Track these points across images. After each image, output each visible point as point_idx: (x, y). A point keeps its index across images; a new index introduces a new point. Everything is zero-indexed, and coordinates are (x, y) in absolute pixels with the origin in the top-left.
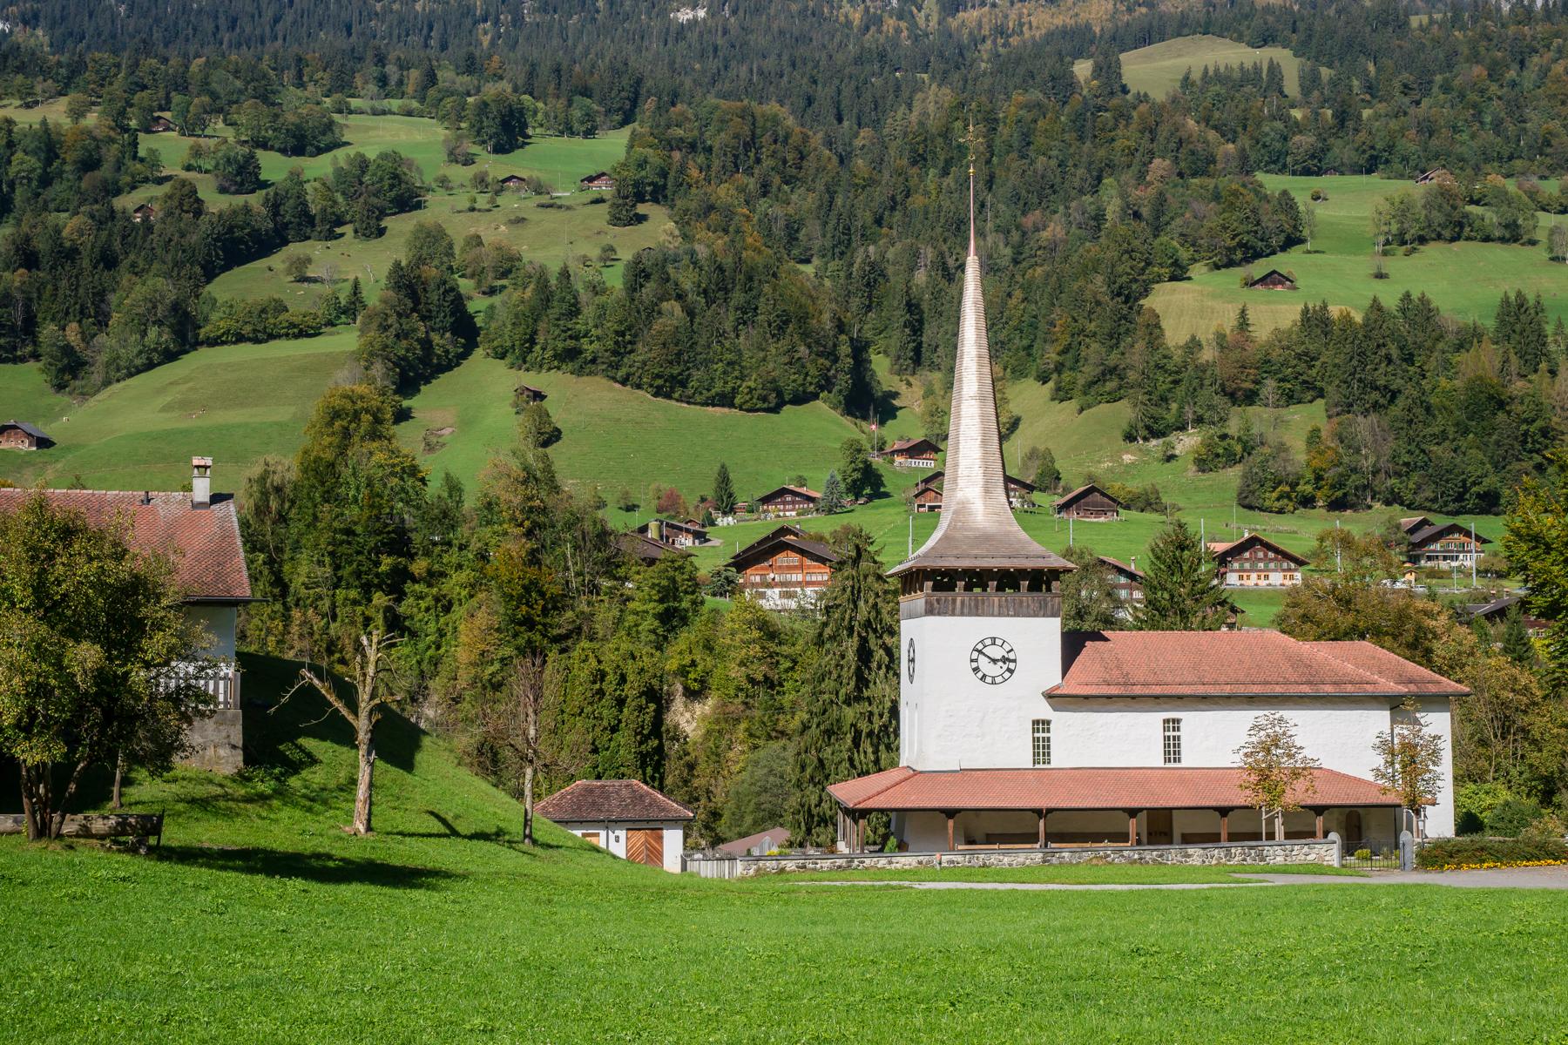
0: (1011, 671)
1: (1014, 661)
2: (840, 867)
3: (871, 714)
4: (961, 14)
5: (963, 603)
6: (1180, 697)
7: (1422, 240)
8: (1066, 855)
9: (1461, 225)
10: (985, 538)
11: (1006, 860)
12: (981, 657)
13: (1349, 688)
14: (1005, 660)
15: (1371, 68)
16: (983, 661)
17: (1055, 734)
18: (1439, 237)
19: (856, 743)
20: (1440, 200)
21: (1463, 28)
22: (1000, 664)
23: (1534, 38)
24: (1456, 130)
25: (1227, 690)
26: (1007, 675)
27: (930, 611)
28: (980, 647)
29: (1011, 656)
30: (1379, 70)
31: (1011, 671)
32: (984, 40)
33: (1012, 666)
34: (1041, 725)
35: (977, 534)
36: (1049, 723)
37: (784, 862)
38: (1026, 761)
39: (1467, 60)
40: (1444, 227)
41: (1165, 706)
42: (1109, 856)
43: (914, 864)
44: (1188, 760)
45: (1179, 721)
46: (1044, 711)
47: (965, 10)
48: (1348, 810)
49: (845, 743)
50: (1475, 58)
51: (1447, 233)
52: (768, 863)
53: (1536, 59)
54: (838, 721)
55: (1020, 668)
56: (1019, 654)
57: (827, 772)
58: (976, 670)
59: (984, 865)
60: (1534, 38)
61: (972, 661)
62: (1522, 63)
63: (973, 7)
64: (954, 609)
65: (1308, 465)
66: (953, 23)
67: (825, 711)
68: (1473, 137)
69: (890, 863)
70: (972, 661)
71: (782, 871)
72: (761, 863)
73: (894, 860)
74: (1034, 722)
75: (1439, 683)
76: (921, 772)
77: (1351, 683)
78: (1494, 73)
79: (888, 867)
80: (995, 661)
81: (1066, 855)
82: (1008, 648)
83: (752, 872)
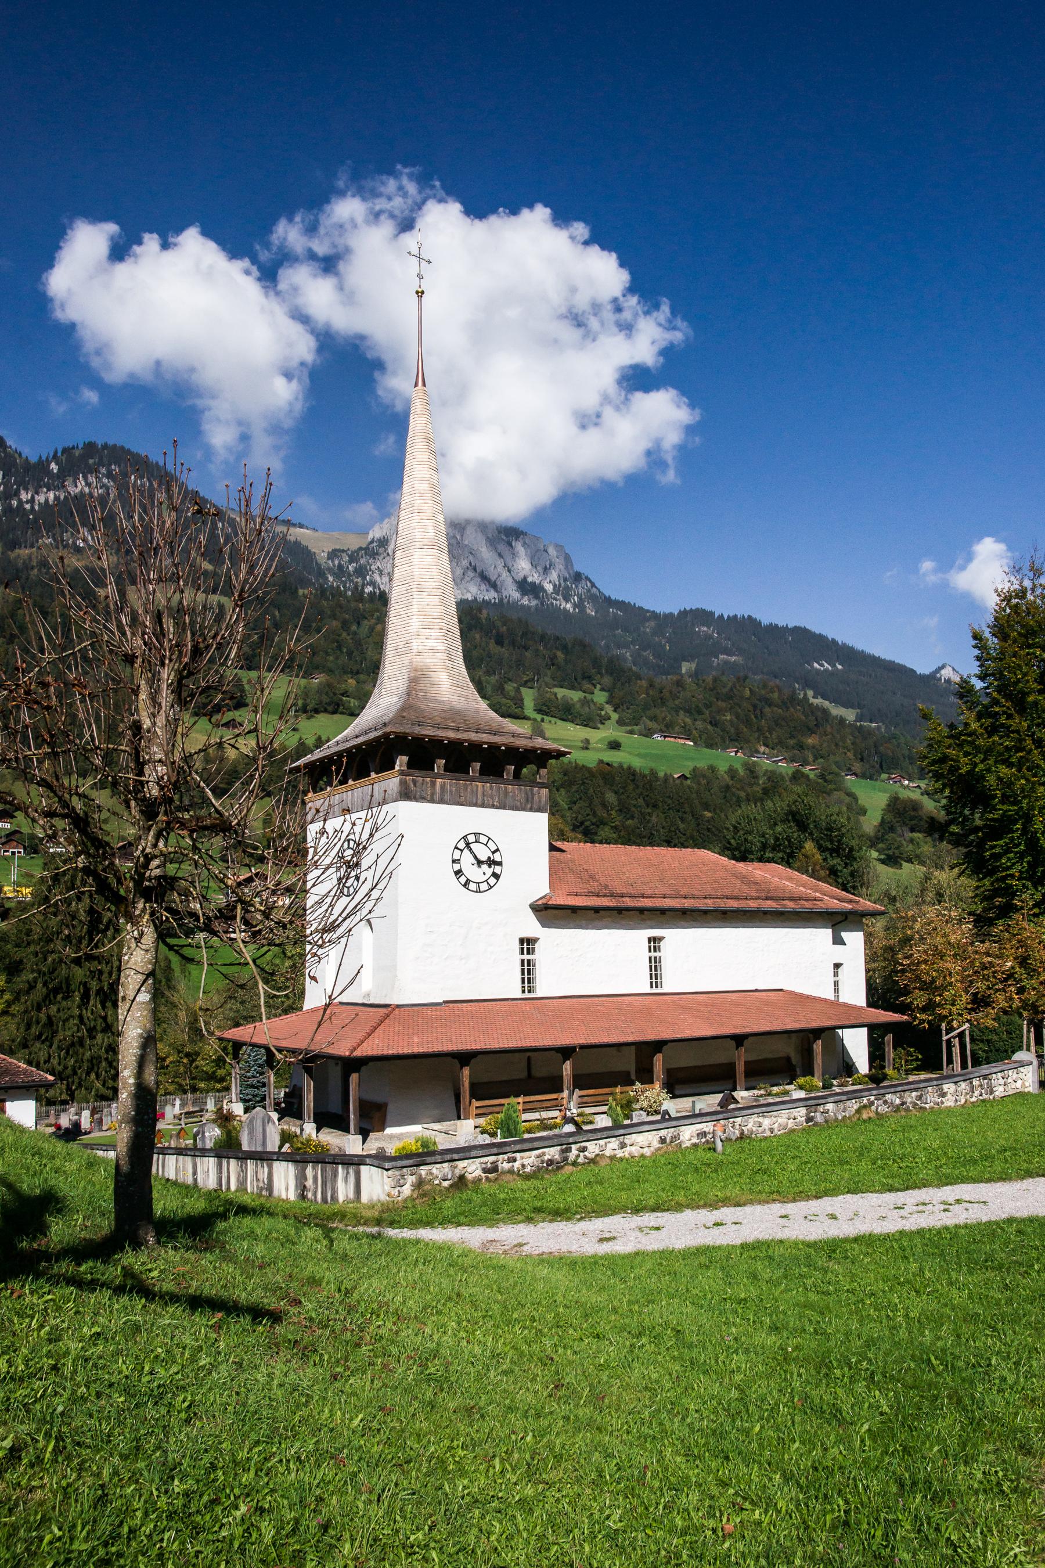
0: (496, 876)
1: (500, 864)
2: (550, 1162)
3: (101, 972)
4: (17, 551)
5: (443, 787)
6: (663, 911)
7: (317, 711)
8: (830, 1107)
9: (338, 705)
10: (453, 714)
11: (766, 1122)
12: (466, 851)
13: (791, 905)
14: (491, 862)
15: (277, 613)
16: (467, 859)
17: (541, 955)
18: (326, 711)
19: (86, 997)
20: (327, 689)
21: (327, 599)
22: (485, 867)
23: (364, 610)
24: (327, 654)
25: (709, 904)
26: (492, 881)
27: (406, 794)
28: (472, 839)
29: (497, 857)
30: (281, 616)
31: (496, 876)
32: (32, 568)
33: (497, 869)
34: (528, 944)
35: (445, 707)
36: (535, 940)
37: (461, 1164)
38: (513, 989)
39: (330, 617)
40: (329, 704)
41: (649, 923)
42: (872, 1103)
43: (656, 1144)
44: (542, 989)
45: (661, 939)
46: (532, 927)
47: (20, 548)
48: (802, 1034)
49: (74, 1002)
50: (334, 617)
51: (330, 709)
52: (435, 1169)
53: (366, 622)
54: (67, 979)
55: (506, 872)
56: (506, 856)
57: (55, 1027)
58: (458, 873)
59: (742, 1137)
60: (364, 610)
61: (454, 861)
62: (359, 623)
63: (26, 547)
64: (433, 794)
65: (264, 837)
66: (12, 555)
67: (54, 970)
68: (337, 658)
69: (623, 1146)
70: (454, 861)
71: (461, 1181)
72: (423, 1171)
73: (628, 1140)
74: (522, 941)
75: (857, 902)
76: (398, 1006)
77: (791, 899)
78: (345, 625)
79: (620, 1154)
80: (480, 863)
81: (830, 1107)
82: (494, 848)
83: (407, 1190)
